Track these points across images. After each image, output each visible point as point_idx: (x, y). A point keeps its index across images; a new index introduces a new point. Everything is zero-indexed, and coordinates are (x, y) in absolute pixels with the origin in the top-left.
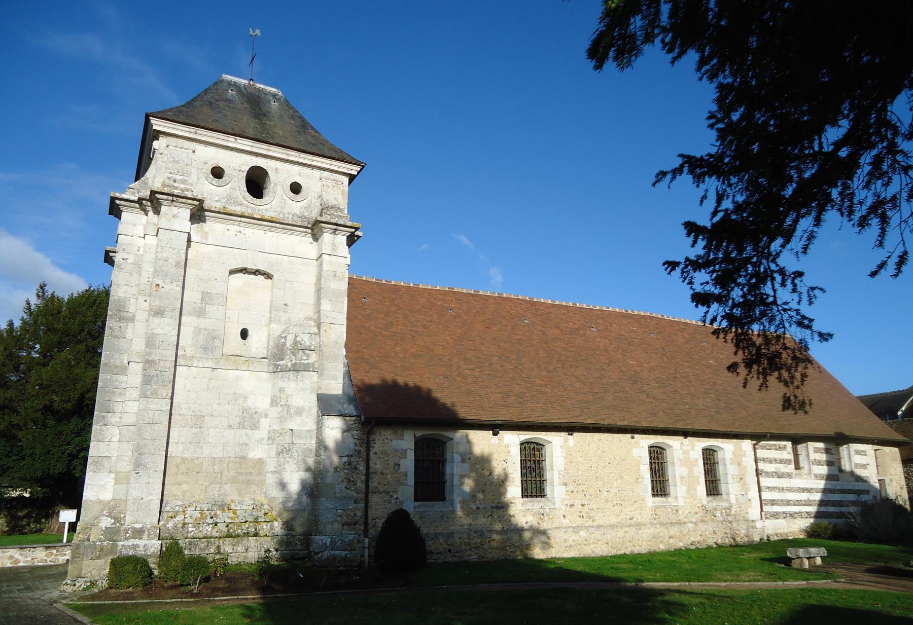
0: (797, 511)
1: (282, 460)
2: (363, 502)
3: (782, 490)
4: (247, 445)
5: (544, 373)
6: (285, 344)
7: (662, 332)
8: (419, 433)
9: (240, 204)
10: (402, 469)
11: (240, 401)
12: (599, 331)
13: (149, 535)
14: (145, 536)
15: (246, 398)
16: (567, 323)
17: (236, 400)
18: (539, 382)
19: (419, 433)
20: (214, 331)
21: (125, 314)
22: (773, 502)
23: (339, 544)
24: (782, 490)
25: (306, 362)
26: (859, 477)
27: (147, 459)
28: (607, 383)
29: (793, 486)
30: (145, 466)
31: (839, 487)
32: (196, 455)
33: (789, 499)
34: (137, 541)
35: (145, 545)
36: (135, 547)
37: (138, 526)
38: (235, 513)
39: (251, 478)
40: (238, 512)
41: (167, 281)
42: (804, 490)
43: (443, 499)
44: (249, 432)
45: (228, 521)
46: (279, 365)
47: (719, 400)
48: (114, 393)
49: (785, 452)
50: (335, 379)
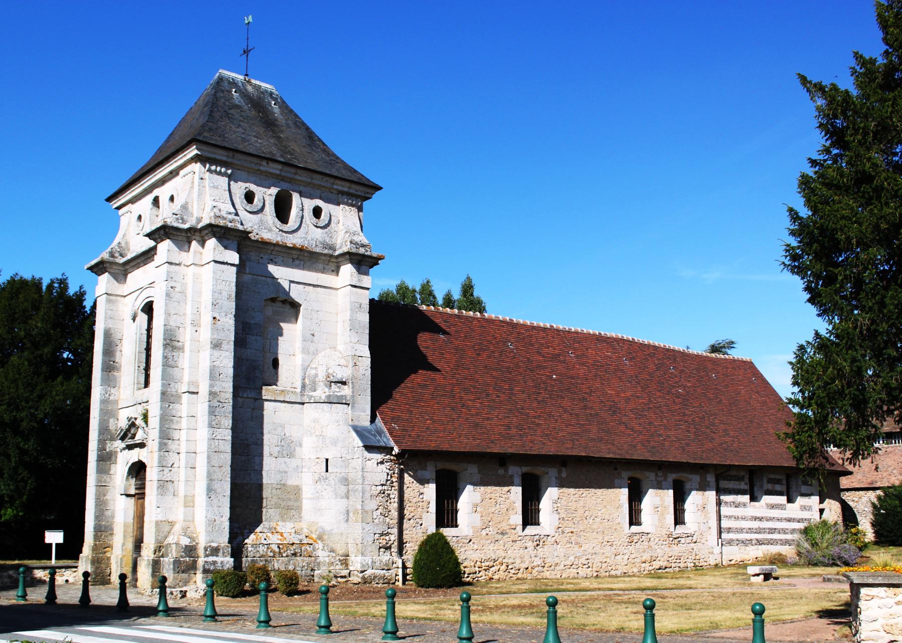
0: (749, 538)
1: (319, 487)
2: (396, 526)
3: (737, 518)
4: (286, 472)
5: (535, 404)
6: (317, 375)
7: (634, 358)
8: (525, 469)
9: (270, 230)
10: (425, 497)
11: (279, 430)
12: (577, 357)
13: (224, 553)
14: (220, 554)
15: (283, 426)
16: (548, 347)
17: (275, 430)
18: (532, 413)
19: (525, 469)
20: (254, 361)
21: (175, 343)
22: (729, 530)
23: (377, 564)
24: (737, 518)
25: (339, 394)
26: (294, 248)
27: (216, 485)
28: (591, 414)
29: (747, 514)
30: (215, 491)
31: (785, 516)
32: (245, 482)
33: (743, 527)
34: (214, 558)
35: (222, 563)
36: (214, 563)
37: (215, 545)
38: (282, 536)
39: (290, 503)
40: (285, 535)
41: (223, 314)
42: (756, 519)
43: (457, 526)
44: (286, 460)
45: (279, 542)
46: (312, 396)
47: (688, 431)
48: (172, 421)
49: (743, 483)
50: (364, 411)
